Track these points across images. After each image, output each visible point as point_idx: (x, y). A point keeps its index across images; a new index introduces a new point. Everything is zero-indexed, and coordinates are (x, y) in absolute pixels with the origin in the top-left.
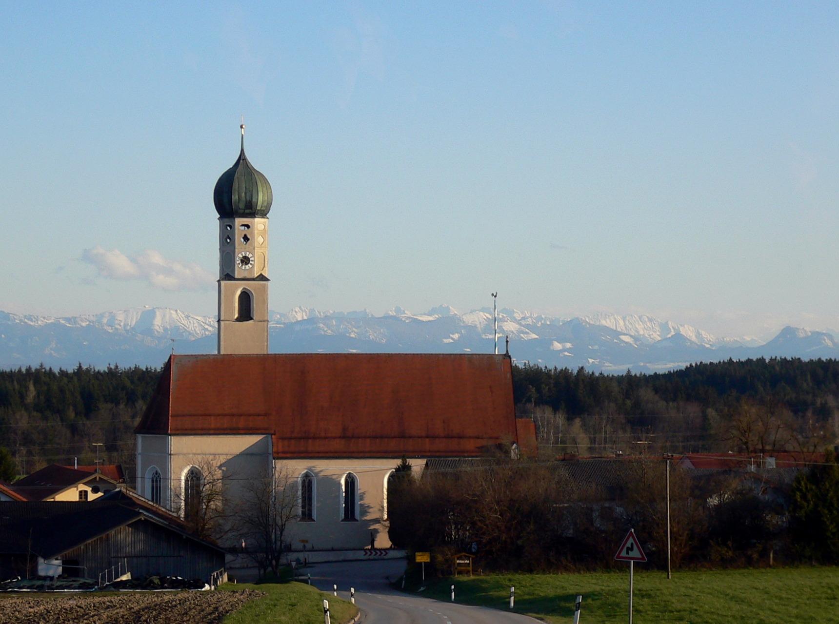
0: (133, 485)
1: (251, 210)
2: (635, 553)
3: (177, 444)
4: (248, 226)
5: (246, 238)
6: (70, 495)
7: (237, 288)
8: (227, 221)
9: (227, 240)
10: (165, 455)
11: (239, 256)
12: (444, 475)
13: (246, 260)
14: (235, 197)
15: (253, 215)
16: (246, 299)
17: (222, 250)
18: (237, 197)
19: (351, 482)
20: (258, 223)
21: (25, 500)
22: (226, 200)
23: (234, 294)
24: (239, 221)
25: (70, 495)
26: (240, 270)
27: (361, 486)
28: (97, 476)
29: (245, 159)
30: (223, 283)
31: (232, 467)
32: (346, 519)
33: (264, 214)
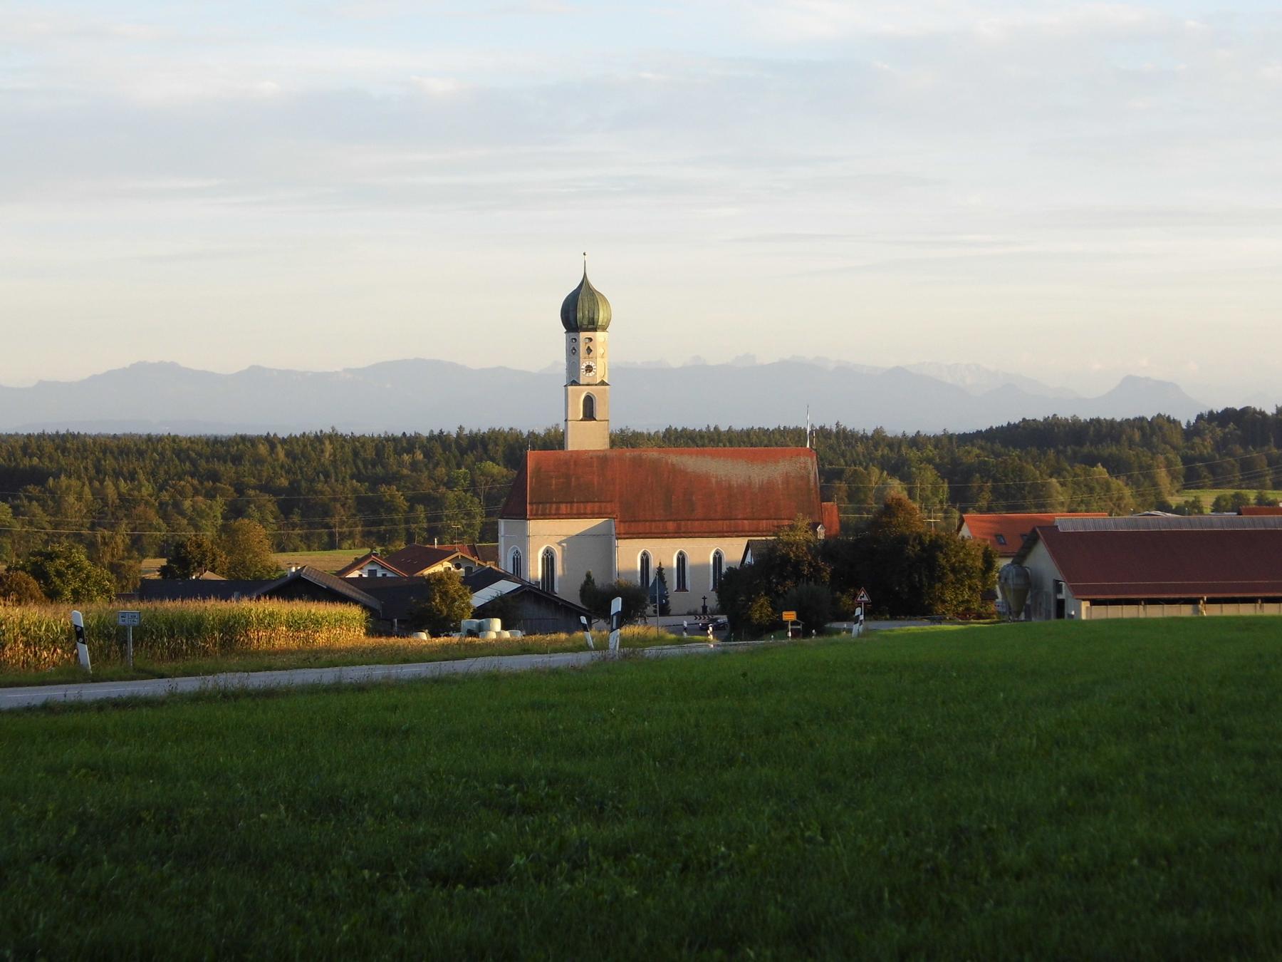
0: (496, 560)
1: (593, 326)
2: (865, 599)
3: (534, 526)
4: (591, 340)
5: (589, 350)
6: (438, 568)
7: (582, 392)
8: (573, 335)
9: (573, 351)
10: (524, 537)
11: (583, 367)
12: (471, 633)
13: (589, 369)
14: (579, 315)
15: (595, 330)
16: (589, 402)
17: (568, 360)
18: (579, 314)
19: (682, 559)
20: (599, 336)
21: (428, 571)
22: (571, 318)
23: (579, 397)
24: (583, 335)
25: (438, 568)
26: (584, 377)
27: (690, 561)
28: (459, 554)
29: (589, 288)
30: (570, 388)
31: (572, 543)
32: (679, 589)
33: (604, 329)
